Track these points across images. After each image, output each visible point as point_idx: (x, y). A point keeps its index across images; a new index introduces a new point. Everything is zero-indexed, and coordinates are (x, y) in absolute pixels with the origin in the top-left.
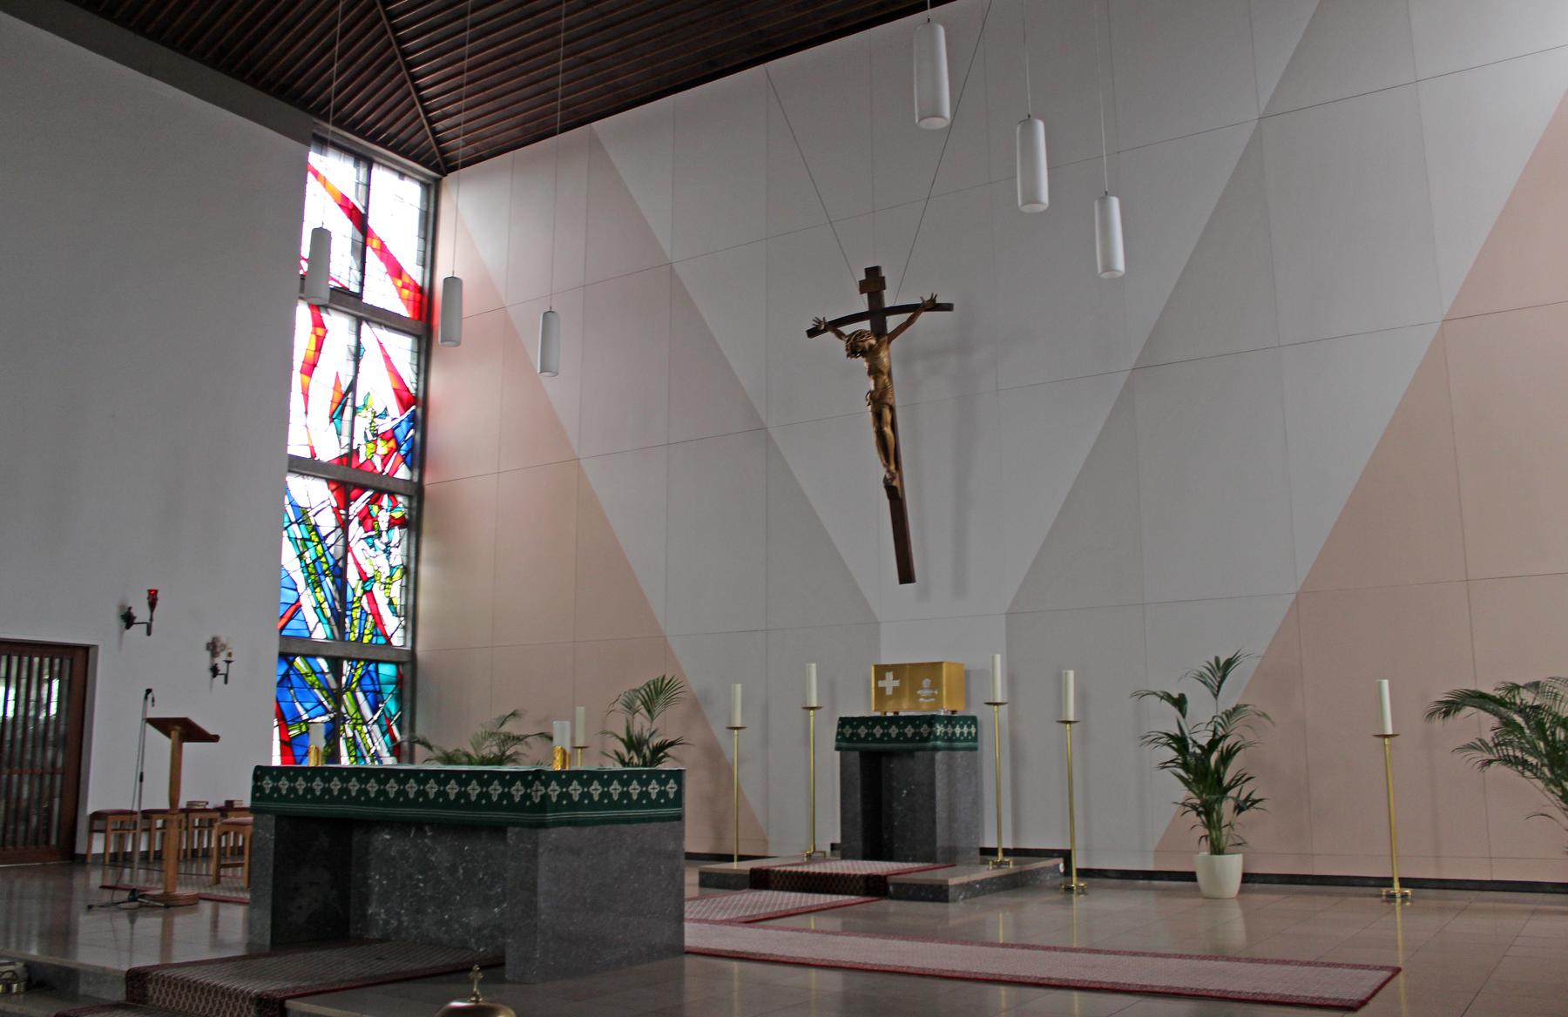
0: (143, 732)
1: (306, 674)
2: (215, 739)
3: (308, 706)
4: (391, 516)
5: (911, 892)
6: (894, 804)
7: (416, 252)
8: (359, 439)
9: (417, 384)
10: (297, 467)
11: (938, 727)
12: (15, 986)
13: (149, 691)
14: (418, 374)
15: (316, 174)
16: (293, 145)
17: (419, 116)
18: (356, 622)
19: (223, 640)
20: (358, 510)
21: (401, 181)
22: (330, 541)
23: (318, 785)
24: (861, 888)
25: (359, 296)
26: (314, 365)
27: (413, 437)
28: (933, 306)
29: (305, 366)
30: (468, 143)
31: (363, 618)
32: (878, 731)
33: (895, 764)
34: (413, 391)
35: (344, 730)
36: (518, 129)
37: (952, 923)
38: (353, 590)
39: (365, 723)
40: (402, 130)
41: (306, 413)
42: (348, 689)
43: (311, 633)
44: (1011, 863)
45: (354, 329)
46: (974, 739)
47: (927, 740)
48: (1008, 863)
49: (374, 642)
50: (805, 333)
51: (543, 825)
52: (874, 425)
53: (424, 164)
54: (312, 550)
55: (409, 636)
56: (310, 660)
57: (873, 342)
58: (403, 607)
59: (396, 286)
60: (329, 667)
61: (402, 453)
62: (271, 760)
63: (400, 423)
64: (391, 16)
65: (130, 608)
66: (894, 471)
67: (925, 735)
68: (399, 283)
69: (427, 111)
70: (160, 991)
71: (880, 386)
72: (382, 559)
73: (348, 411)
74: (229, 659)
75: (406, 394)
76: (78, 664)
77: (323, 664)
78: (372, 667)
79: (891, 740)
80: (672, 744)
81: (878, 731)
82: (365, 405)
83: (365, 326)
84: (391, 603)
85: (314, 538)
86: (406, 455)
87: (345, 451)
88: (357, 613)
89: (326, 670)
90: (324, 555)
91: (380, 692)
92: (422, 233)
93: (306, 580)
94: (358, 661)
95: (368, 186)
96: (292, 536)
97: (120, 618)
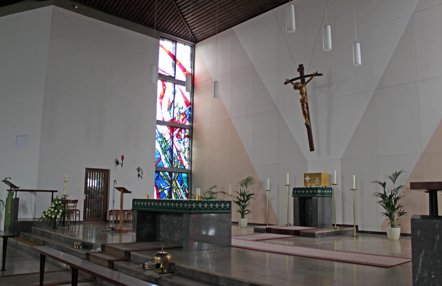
0: (114, 190)
1: (163, 176)
2: (131, 192)
3: (164, 184)
4: (184, 135)
5: (306, 235)
6: (309, 212)
7: (190, 65)
8: (175, 115)
9: (191, 100)
10: (159, 123)
11: (319, 190)
12: (80, 247)
13: (115, 181)
14: (191, 97)
15: (162, 47)
16: (156, 40)
17: (187, 29)
18: (176, 163)
19: (141, 168)
20: (176, 134)
21: (185, 46)
22: (168, 142)
23: (156, 204)
24: (293, 233)
25: (174, 78)
26: (163, 96)
27: (190, 114)
28: (317, 74)
29: (161, 96)
30: (201, 35)
31: (178, 161)
32: (307, 192)
33: (309, 201)
34: (190, 102)
35: (173, 191)
36: (213, 30)
37: (316, 243)
38: (175, 154)
39: (179, 189)
40: (183, 33)
41: (161, 109)
42: (174, 180)
43: (164, 166)
44: (338, 228)
45: (173, 86)
46: (330, 195)
47: (315, 194)
48: (338, 228)
49: (181, 168)
50: (323, 75)
51: (191, 213)
52: (302, 108)
53: (191, 41)
54: (164, 144)
55: (190, 166)
56: (164, 173)
57: (301, 85)
58: (188, 159)
59: (184, 74)
60: (169, 174)
61: (187, 118)
62: (154, 198)
63: (186, 110)
64: (177, 4)
65: (118, 160)
66: (308, 121)
67: (315, 193)
68: (185, 73)
69: (189, 27)
70: (107, 249)
71: (303, 97)
72: (182, 146)
73: (172, 108)
74: (142, 173)
75: (188, 102)
76: (106, 173)
77: (167, 173)
78: (180, 174)
79: (306, 194)
80: (252, 195)
81: (303, 192)
82: (177, 106)
83: (176, 85)
84: (185, 157)
85: (164, 141)
86: (188, 118)
87: (172, 118)
88: (176, 160)
89: (168, 175)
90: (167, 145)
91: (183, 181)
92: (191, 59)
93: (163, 152)
94: (177, 173)
95: (176, 48)
96: (159, 141)
97: (115, 163)
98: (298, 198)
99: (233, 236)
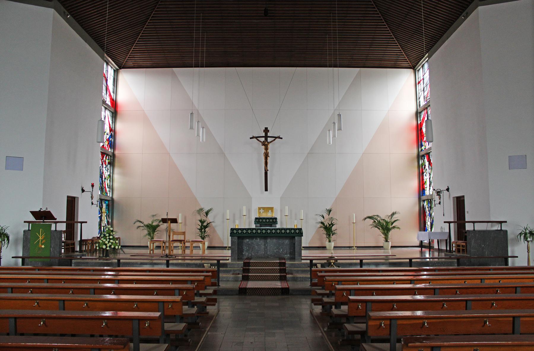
28: (279, 138)
30: (133, 64)
52: (265, 160)
53: (117, 65)
84: (107, 185)
98: (171, 224)
99: (306, 248)
